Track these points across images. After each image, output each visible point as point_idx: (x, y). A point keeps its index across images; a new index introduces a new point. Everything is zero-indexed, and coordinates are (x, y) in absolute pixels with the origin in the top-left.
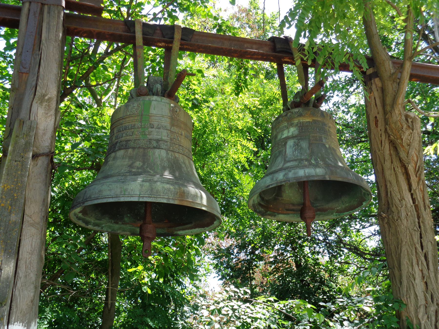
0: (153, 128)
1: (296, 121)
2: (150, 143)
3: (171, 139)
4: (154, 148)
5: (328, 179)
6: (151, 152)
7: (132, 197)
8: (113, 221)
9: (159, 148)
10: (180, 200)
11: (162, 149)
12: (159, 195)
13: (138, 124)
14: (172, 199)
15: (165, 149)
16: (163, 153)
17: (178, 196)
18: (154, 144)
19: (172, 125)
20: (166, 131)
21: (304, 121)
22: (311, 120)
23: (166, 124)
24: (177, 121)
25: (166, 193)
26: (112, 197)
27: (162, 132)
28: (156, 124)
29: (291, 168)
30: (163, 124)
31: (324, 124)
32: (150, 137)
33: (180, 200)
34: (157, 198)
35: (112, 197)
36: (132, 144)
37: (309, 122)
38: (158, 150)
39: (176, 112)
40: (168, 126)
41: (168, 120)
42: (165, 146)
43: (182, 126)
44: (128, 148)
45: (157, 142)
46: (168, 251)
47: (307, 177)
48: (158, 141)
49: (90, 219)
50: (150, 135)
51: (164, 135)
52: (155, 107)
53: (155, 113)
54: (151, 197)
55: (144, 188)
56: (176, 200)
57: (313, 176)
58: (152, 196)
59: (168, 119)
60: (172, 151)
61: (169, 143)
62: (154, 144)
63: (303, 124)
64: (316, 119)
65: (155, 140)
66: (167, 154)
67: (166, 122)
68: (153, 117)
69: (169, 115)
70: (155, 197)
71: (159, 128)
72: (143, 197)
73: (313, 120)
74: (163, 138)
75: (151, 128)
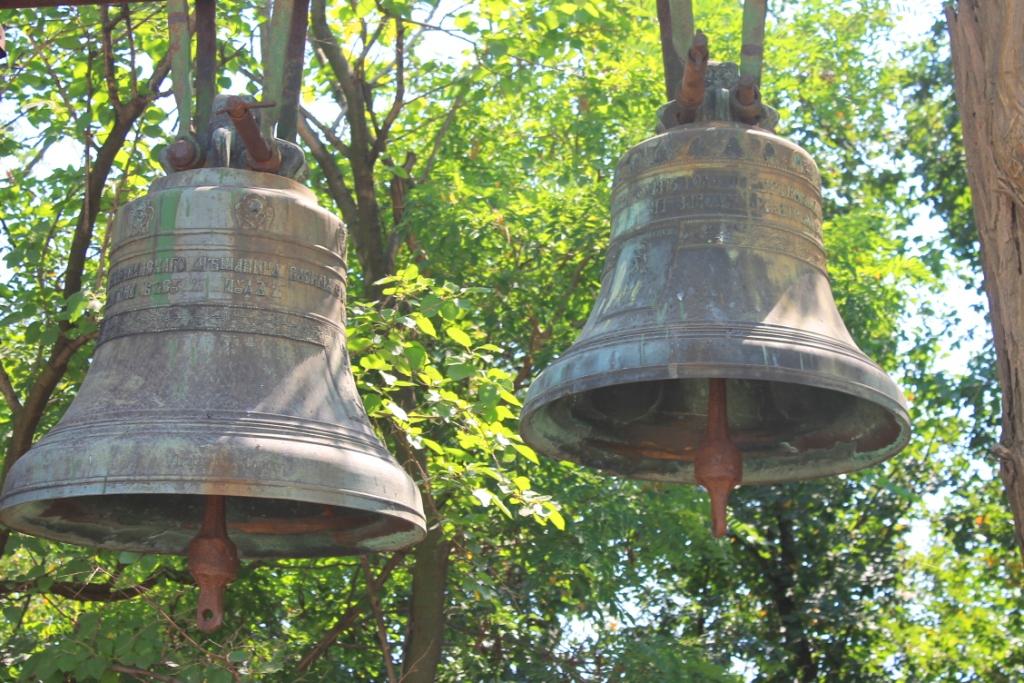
0: (184, 270)
1: (647, 181)
2: (174, 316)
3: (235, 296)
4: (183, 330)
5: (675, 376)
6: (171, 342)
7: (88, 483)
8: (178, 524)
9: (196, 330)
10: (216, 482)
11: (205, 330)
12: (155, 474)
13: (147, 263)
14: (192, 481)
15: (214, 331)
16: (206, 341)
17: (210, 472)
18: (184, 317)
19: (241, 252)
20: (219, 275)
21: (670, 176)
22: (690, 173)
23: (220, 254)
24: (260, 236)
25: (176, 466)
26: (48, 487)
27: (207, 280)
28: (190, 257)
29: (621, 337)
30: (210, 254)
31: (735, 179)
32: (172, 299)
33: (216, 482)
34: (148, 482)
35: (48, 487)
36: (130, 324)
37: (683, 178)
38: (192, 335)
39: (256, 211)
40: (227, 257)
41: (228, 241)
42: (213, 321)
43: (280, 248)
44: (122, 337)
45: (193, 313)
46: (959, 507)
47: (620, 373)
48: (194, 308)
49: (99, 526)
50: (174, 292)
51: (215, 287)
52: (188, 208)
53: (188, 225)
54: (135, 481)
55: (119, 457)
56: (206, 481)
57: (632, 371)
58: (138, 478)
59: (226, 238)
60: (233, 332)
61: (226, 311)
62: (184, 317)
63: (664, 189)
64: (707, 165)
65: (186, 306)
66: (220, 343)
67: (221, 247)
68: (184, 238)
69: (231, 224)
70: (143, 481)
71: (200, 270)
72: (115, 482)
73: (698, 171)
74: (211, 296)
75: (179, 271)
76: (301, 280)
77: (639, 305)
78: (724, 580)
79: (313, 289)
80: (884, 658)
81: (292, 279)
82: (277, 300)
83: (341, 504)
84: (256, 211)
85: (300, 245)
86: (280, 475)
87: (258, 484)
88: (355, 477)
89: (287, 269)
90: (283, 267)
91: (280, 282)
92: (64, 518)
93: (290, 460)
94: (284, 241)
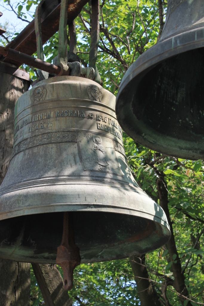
8: (107, 245)
76: (62, 115)
77: (104, 6)
78: (46, 156)
79: (71, 118)
80: (73, 305)
81: (58, 116)
82: (50, 128)
83: (53, 211)
84: (39, 93)
85: (61, 101)
86: (21, 205)
87: (10, 212)
88: (63, 196)
89: (55, 112)
90: (52, 113)
91: (51, 120)
92: (50, 253)
93: (26, 196)
94: (52, 101)
